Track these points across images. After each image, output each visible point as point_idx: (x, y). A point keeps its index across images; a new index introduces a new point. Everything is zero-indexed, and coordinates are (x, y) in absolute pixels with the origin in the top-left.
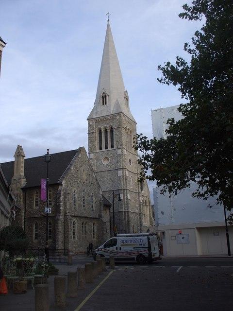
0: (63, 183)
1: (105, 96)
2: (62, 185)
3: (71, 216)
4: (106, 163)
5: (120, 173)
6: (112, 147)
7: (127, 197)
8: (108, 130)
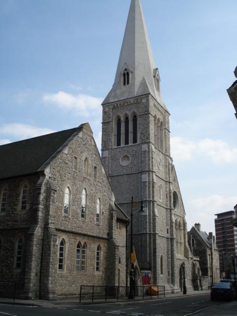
0: (47, 171)
1: (128, 74)
2: (44, 175)
3: (58, 230)
4: (125, 163)
5: (145, 177)
6: (135, 141)
7: (154, 212)
8: (130, 119)
